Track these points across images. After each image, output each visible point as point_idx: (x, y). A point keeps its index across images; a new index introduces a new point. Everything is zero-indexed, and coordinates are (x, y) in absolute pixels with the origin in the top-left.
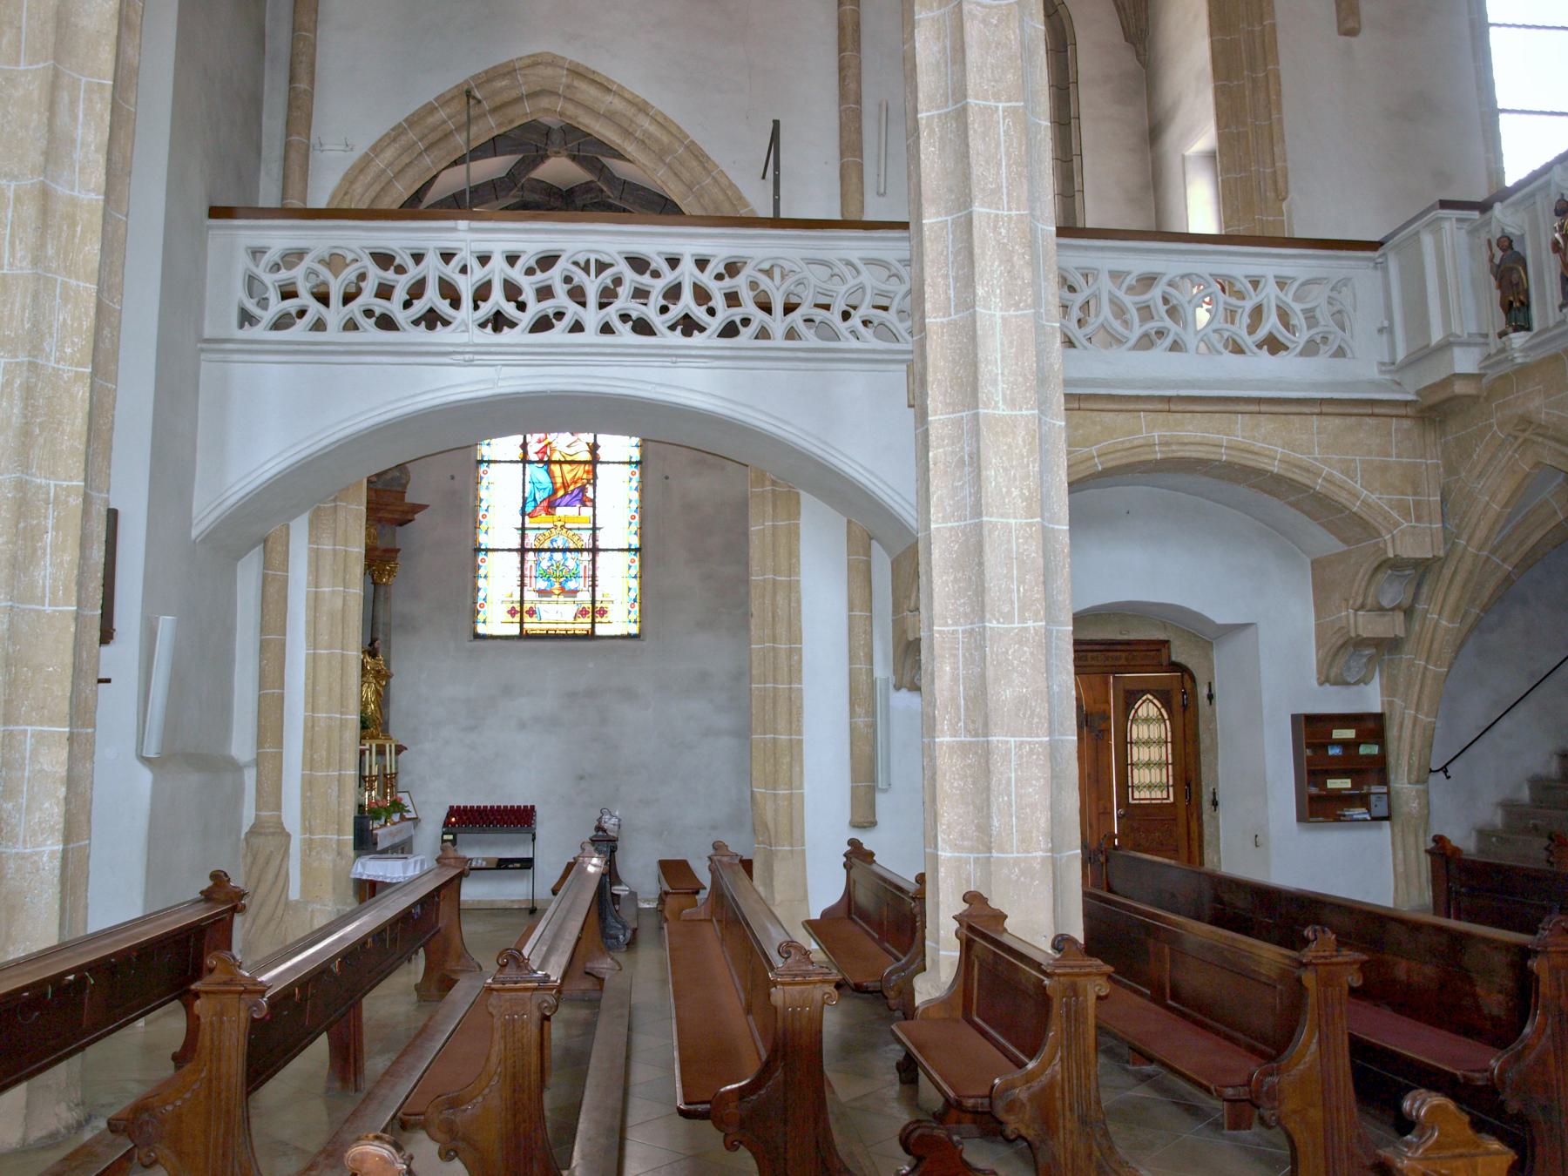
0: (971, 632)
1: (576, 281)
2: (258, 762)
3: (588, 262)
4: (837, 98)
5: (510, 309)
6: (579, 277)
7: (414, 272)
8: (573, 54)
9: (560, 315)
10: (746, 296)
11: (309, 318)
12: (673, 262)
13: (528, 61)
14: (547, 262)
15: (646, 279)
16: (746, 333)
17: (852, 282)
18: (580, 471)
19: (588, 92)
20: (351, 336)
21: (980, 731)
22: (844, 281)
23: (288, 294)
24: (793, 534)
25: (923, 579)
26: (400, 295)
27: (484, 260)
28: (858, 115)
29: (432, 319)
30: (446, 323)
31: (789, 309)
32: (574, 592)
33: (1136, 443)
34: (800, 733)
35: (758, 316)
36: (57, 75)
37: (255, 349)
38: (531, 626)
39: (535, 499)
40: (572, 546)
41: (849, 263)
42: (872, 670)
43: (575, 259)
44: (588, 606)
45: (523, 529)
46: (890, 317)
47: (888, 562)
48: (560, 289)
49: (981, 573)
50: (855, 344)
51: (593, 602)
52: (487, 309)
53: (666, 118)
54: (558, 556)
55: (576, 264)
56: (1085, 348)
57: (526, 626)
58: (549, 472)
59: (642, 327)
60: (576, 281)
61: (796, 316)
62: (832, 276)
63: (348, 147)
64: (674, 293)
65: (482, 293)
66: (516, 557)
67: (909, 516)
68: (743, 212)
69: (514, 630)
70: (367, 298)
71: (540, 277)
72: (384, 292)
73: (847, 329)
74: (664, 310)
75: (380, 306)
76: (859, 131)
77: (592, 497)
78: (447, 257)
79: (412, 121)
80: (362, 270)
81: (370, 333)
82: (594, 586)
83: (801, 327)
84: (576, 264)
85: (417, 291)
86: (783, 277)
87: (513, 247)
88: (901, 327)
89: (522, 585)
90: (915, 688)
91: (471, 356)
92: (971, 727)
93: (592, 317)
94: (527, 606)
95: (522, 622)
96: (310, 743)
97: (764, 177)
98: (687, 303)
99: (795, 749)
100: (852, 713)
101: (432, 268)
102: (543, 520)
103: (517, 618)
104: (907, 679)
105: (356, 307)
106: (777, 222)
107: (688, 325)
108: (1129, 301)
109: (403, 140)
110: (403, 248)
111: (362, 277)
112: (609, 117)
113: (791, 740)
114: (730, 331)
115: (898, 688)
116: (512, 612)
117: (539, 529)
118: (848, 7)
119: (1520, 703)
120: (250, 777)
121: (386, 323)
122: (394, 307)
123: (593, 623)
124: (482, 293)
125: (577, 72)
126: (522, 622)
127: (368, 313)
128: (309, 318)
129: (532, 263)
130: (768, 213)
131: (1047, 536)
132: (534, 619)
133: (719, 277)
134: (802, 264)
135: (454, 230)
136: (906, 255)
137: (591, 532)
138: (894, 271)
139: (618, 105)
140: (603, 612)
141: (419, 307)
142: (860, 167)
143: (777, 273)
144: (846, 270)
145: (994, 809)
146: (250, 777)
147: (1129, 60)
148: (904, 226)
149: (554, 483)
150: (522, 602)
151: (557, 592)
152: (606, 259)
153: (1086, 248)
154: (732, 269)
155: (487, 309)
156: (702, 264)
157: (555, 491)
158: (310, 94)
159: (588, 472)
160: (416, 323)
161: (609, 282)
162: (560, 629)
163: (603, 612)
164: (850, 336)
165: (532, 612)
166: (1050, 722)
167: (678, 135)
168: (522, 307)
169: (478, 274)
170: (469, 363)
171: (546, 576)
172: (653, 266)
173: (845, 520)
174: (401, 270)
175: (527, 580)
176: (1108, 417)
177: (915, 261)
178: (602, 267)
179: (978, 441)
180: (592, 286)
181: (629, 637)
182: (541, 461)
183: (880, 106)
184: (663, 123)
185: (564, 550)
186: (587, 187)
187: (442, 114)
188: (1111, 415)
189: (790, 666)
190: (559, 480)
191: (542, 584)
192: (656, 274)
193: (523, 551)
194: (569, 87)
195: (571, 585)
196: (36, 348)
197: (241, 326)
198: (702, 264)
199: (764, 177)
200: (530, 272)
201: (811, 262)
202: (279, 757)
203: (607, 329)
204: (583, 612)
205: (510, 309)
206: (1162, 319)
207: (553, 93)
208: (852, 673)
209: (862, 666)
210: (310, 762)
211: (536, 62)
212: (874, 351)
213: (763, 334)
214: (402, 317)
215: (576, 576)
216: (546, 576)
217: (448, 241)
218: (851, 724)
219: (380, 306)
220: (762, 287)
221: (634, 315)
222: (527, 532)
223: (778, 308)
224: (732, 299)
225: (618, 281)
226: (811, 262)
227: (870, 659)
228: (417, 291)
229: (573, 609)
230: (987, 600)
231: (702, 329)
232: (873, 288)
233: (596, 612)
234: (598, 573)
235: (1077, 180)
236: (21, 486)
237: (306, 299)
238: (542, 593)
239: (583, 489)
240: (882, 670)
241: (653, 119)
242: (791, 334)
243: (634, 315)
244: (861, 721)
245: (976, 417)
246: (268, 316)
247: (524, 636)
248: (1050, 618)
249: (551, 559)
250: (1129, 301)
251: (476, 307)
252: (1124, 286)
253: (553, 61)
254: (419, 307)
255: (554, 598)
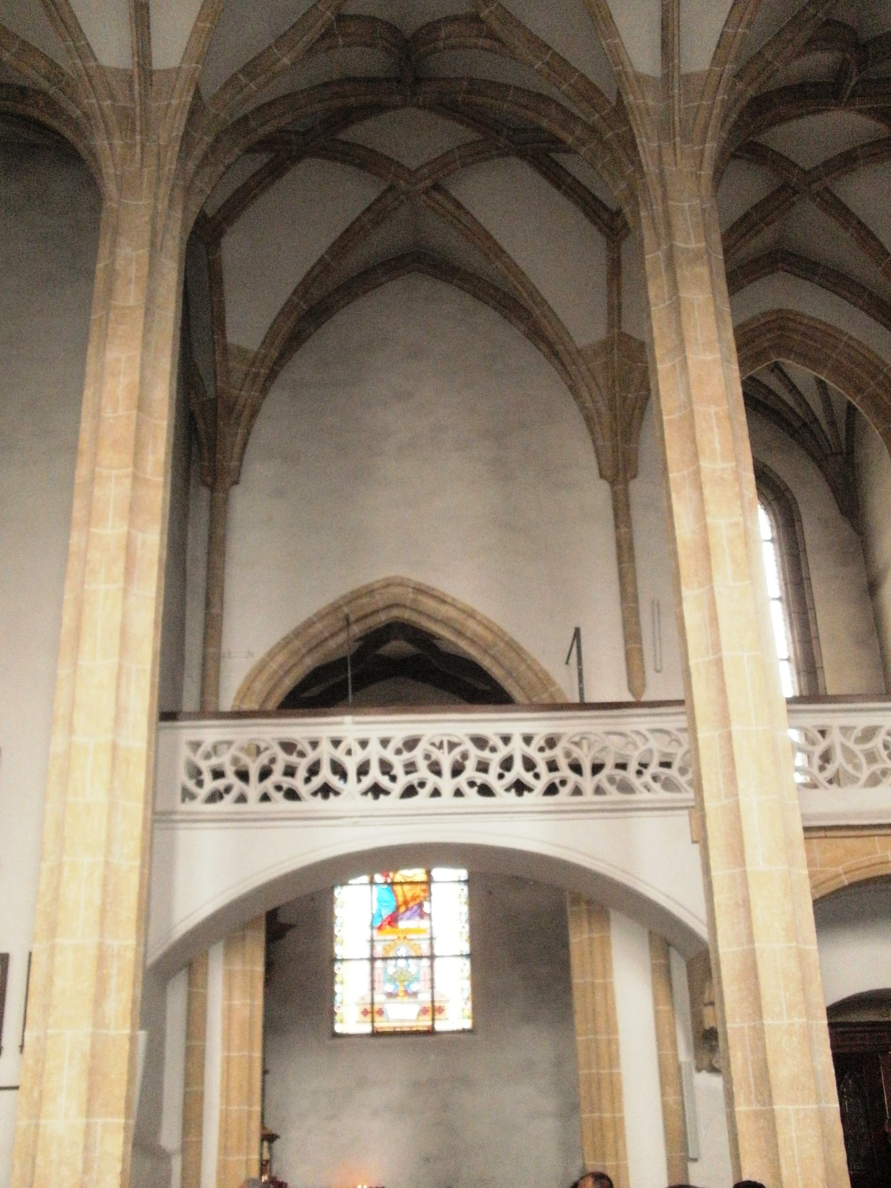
0: (754, 1027)
1: (434, 757)
2: (185, 1148)
3: (441, 743)
4: (618, 599)
5: (384, 781)
6: (436, 754)
7: (312, 756)
8: (417, 576)
9: (422, 784)
10: (563, 763)
11: (234, 794)
12: (506, 740)
13: (383, 584)
14: (411, 744)
15: (486, 754)
16: (564, 791)
17: (643, 748)
18: (418, 890)
19: (429, 604)
20: (266, 806)
21: (767, 1101)
22: (636, 747)
23: (218, 774)
24: (606, 943)
25: (714, 975)
26: (302, 773)
27: (364, 744)
28: (636, 612)
29: (326, 791)
30: (337, 793)
31: (597, 768)
32: (415, 994)
33: (873, 861)
34: (621, 1110)
35: (572, 777)
36: (120, 667)
37: (195, 819)
38: (382, 1024)
39: (381, 916)
40: (413, 954)
41: (638, 733)
42: (677, 1055)
43: (432, 741)
44: (429, 1005)
45: (372, 941)
46: (673, 772)
47: (683, 965)
48: (422, 765)
49: (757, 984)
50: (646, 795)
51: (433, 1002)
52: (367, 781)
53: (490, 621)
54: (402, 963)
55: (433, 744)
56: (826, 788)
57: (377, 1025)
58: (394, 892)
59: (485, 791)
60: (434, 757)
61: (602, 776)
62: (627, 744)
63: (250, 654)
64: (507, 764)
65: (363, 770)
66: (367, 964)
67: (702, 931)
68: (560, 701)
69: (367, 1029)
70: (277, 776)
71: (406, 756)
72: (290, 772)
73: (641, 784)
74: (501, 776)
75: (287, 782)
76: (638, 623)
77: (428, 912)
78: (336, 743)
79: (297, 633)
80: (273, 756)
81: (280, 803)
82: (432, 987)
83: (606, 785)
84: (433, 744)
85: (314, 770)
86: (589, 747)
87: (385, 734)
88: (682, 780)
89: (373, 989)
90: (713, 1070)
91: (357, 819)
92: (760, 1097)
93: (447, 784)
94: (376, 1007)
95: (373, 1022)
96: (225, 1132)
97: (567, 663)
98: (518, 770)
99: (618, 1125)
100: (663, 1094)
101: (326, 752)
102: (389, 935)
103: (369, 1018)
104: (705, 1063)
105: (269, 784)
106: (583, 706)
107: (520, 787)
108: (857, 748)
109: (291, 647)
110: (304, 738)
111: (273, 760)
112: (445, 622)
113: (614, 1117)
114: (552, 790)
115: (699, 1070)
116: (365, 1012)
117: (385, 940)
118: (623, 530)
119: (268, 1087)
120: (176, 1164)
121: (292, 795)
122: (297, 783)
123: (433, 1020)
124: (363, 770)
125: (420, 590)
126: (373, 1022)
127: (279, 788)
128: (234, 794)
129: (400, 745)
130: (576, 699)
131: (801, 956)
132: (383, 1018)
133: (541, 749)
134: (604, 736)
135: (341, 723)
136: (685, 725)
137: (429, 942)
138: (673, 737)
139: (452, 613)
140: (441, 1010)
141: (317, 782)
142: (640, 650)
143: (585, 743)
144: (638, 739)
145: (782, 1161)
146: (176, 1164)
147: (846, 530)
148: (680, 703)
149: (397, 901)
150: (372, 1004)
151: (401, 994)
152: (455, 740)
153: (821, 711)
154: (551, 742)
155: (367, 781)
156: (528, 740)
157: (398, 908)
158: (221, 616)
159: (424, 891)
160: (315, 794)
161: (459, 758)
162: (406, 1026)
163: (441, 1010)
164: (643, 789)
165: (381, 1012)
166: (818, 1095)
167: (499, 634)
168: (393, 779)
169: (359, 755)
170: (356, 824)
171: (392, 979)
172: (491, 743)
173: (647, 931)
174: (302, 754)
175: (376, 985)
176: (848, 842)
177: (692, 729)
178: (452, 746)
179: (747, 890)
180: (446, 761)
181: (464, 1031)
182: (386, 883)
183: (653, 603)
184: (488, 626)
185: (407, 958)
186: (416, 659)
187: (319, 626)
188: (851, 840)
189: (610, 1054)
190: (401, 899)
191: (390, 988)
192: (493, 750)
193: (373, 959)
194: (414, 600)
195: (414, 987)
196: (108, 852)
197: (183, 800)
198: (528, 740)
199: (567, 663)
200: (398, 752)
201: (609, 733)
202: (199, 1143)
203: (458, 793)
204: (424, 1011)
205: (384, 781)
206: (884, 761)
207: (404, 606)
208: (660, 1058)
209: (669, 1052)
210: (224, 1149)
211: (388, 584)
212: (662, 801)
213: (577, 791)
214: (303, 790)
215: (417, 979)
216: (392, 979)
217: (335, 732)
218: (663, 1103)
219: (286, 782)
220: (574, 755)
221: (479, 782)
222: (375, 943)
223: (587, 769)
224: (552, 766)
225: (465, 756)
226: (609, 733)
227: (674, 1043)
228: (314, 770)
229: (417, 1008)
230: (763, 1003)
231: (530, 790)
232: (659, 751)
233: (434, 1010)
234: (436, 977)
235: (812, 627)
236: (101, 947)
237: (231, 778)
238: (390, 995)
239: (421, 905)
240: (685, 1055)
241: (480, 623)
242: (599, 790)
243: (479, 782)
244: (672, 1099)
245: (745, 872)
246: (204, 793)
247: (376, 1034)
248: (809, 1014)
249: (396, 965)
250: (857, 748)
251: (359, 781)
252: (853, 738)
253: (402, 583)
254: (317, 782)
255: (399, 999)
